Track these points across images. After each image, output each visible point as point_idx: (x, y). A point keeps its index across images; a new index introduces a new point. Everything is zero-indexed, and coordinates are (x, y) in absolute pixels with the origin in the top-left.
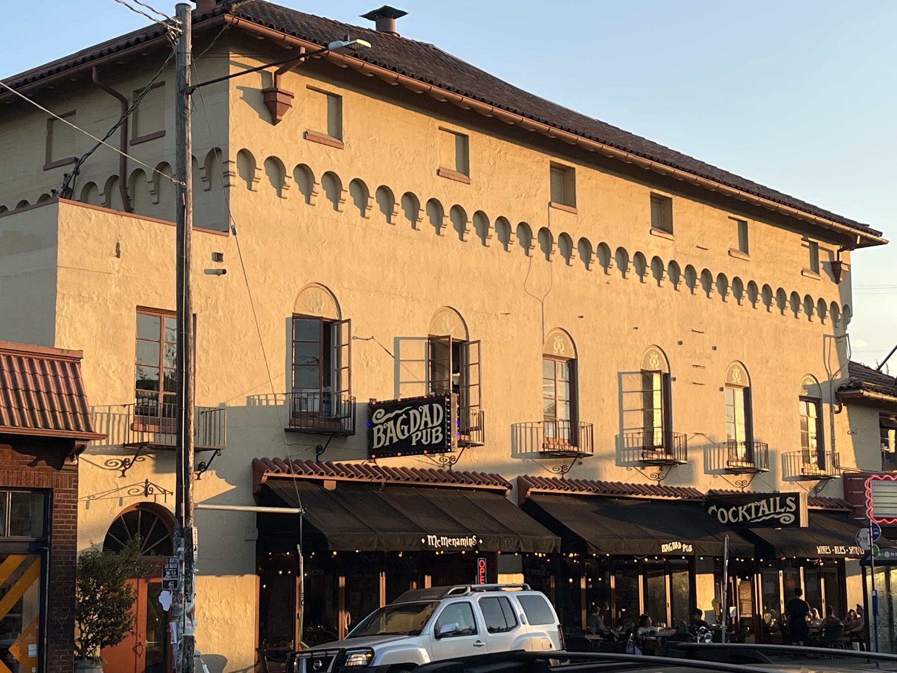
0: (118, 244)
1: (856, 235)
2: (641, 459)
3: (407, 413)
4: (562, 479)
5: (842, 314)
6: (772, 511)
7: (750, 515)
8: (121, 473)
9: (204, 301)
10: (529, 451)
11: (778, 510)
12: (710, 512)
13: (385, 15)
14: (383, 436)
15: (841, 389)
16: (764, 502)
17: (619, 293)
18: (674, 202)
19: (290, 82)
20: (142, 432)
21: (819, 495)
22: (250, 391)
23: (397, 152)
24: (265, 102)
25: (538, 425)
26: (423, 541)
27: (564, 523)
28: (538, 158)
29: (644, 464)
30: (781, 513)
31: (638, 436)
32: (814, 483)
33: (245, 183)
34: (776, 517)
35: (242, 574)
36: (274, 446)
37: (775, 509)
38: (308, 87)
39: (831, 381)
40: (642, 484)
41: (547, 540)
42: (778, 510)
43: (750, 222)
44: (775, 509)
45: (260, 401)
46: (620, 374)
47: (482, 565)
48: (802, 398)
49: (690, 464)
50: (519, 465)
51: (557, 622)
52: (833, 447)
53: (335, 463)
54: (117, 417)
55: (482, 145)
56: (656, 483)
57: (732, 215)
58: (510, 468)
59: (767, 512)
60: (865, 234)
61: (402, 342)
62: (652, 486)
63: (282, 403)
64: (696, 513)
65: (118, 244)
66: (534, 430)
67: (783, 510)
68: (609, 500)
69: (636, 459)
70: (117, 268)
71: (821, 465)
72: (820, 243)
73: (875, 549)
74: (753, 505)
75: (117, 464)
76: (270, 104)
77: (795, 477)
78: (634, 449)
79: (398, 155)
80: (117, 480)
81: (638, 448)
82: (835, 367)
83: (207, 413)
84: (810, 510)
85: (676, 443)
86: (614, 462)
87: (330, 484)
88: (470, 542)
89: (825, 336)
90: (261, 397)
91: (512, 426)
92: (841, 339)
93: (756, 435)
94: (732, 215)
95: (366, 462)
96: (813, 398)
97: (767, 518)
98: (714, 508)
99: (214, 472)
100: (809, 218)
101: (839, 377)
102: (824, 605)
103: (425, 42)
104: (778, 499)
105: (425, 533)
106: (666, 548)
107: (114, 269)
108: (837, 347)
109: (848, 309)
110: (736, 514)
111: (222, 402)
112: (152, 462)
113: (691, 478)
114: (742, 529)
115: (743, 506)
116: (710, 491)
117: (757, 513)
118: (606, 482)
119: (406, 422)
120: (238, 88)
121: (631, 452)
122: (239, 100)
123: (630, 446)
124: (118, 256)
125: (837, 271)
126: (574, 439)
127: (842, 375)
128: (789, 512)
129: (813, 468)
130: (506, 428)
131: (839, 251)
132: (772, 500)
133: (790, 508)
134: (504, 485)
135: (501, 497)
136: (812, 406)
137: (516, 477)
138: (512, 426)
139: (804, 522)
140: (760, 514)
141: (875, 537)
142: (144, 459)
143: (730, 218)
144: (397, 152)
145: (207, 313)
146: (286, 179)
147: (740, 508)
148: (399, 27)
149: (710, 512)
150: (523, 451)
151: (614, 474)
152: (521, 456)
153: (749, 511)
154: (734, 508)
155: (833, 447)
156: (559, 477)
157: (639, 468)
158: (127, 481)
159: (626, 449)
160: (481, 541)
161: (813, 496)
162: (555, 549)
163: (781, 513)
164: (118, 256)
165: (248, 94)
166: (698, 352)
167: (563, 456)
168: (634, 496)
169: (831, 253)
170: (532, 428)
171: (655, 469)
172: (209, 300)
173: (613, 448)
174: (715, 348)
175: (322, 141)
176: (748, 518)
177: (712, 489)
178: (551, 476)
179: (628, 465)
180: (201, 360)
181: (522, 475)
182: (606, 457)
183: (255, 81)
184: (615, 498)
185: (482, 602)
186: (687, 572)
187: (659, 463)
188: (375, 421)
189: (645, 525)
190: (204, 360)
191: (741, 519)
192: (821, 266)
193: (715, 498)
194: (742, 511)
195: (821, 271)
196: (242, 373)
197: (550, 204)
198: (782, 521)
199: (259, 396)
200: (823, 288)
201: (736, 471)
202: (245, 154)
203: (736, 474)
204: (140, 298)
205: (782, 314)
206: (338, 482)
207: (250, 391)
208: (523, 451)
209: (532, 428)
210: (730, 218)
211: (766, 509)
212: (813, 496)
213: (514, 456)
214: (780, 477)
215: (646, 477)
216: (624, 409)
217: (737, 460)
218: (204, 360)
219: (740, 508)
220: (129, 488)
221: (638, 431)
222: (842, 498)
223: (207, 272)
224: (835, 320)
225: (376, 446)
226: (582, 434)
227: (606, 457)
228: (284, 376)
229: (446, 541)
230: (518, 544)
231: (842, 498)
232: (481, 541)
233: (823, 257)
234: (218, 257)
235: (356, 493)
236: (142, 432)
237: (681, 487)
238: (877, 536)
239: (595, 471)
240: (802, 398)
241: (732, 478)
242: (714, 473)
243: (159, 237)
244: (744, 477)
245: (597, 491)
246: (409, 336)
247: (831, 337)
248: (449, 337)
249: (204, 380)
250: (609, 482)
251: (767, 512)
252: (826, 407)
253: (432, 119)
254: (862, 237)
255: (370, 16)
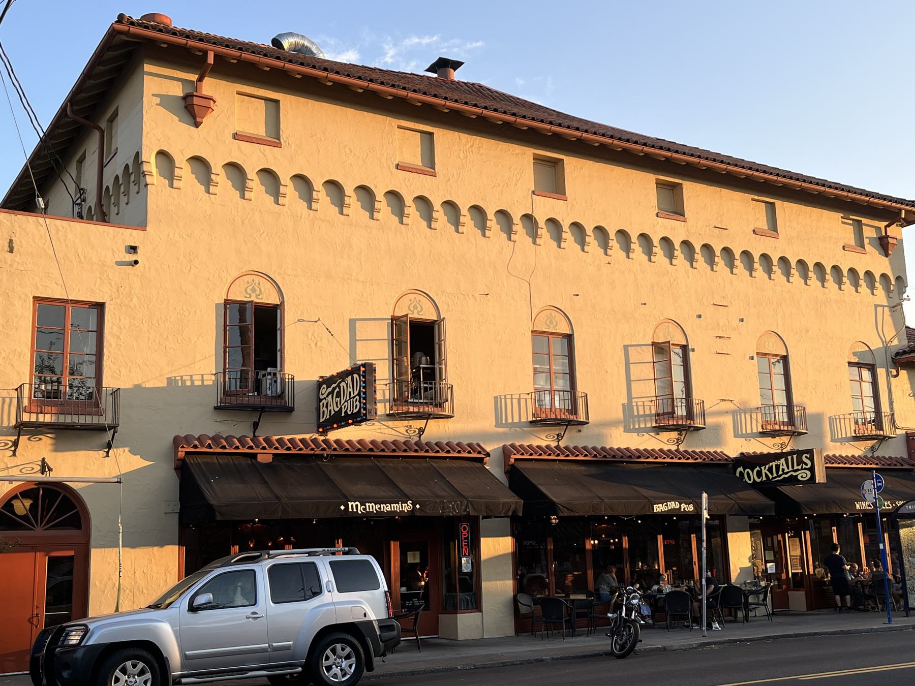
0: (11, 241)
1: (900, 210)
2: (654, 425)
3: (339, 386)
4: (558, 447)
5: (896, 285)
6: (791, 469)
7: (772, 474)
8: (11, 453)
9: (115, 290)
10: (516, 420)
11: (796, 467)
12: (738, 475)
13: (443, 65)
14: (325, 409)
15: (897, 354)
16: (783, 461)
17: (623, 272)
18: (684, 187)
19: (211, 86)
20: (37, 413)
21: (876, 455)
22: (171, 372)
23: (347, 149)
24: (186, 107)
25: (527, 396)
26: (342, 508)
27: (542, 488)
28: (517, 151)
29: (659, 429)
30: (798, 470)
31: (650, 404)
32: (870, 443)
33: (166, 182)
34: (794, 474)
35: (162, 545)
36: (204, 425)
37: (793, 467)
38: (239, 93)
39: (886, 348)
40: (657, 449)
41: (504, 503)
42: (796, 467)
43: (778, 203)
44: (793, 467)
45: (183, 382)
46: (626, 348)
47: (465, 531)
48: (851, 364)
49: (717, 428)
50: (504, 433)
51: (384, 586)
52: (892, 409)
53: (287, 437)
54: (8, 400)
55: (447, 140)
56: (674, 448)
57: (756, 197)
58: (490, 437)
59: (786, 470)
60: (909, 208)
61: (358, 324)
62: (669, 451)
63: (211, 383)
64: (718, 473)
65: (11, 241)
66: (523, 402)
67: (800, 467)
68: (611, 466)
69: (649, 425)
70: (9, 263)
71: (880, 427)
72: (864, 221)
73: (880, 500)
74: (774, 464)
75: (6, 444)
76: (191, 109)
77: (846, 438)
78: (645, 416)
79: (348, 152)
80: (6, 460)
81: (650, 415)
82: (890, 332)
83: (116, 392)
84: (826, 468)
85: (696, 409)
86: (621, 429)
87: (265, 457)
88: (407, 507)
89: (876, 306)
90: (184, 378)
91: (496, 398)
92: (896, 309)
93: (796, 400)
94: (756, 197)
95: (316, 436)
96: (865, 364)
97: (786, 476)
98: (741, 469)
99: (127, 449)
100: (859, 200)
101: (896, 342)
102: (889, 559)
103: (472, 82)
104: (795, 456)
105: (346, 500)
106: (659, 508)
107: (6, 263)
108: (892, 316)
109: (901, 281)
110: (759, 474)
111: (137, 383)
112: (49, 441)
113: (719, 441)
114: (767, 488)
115: (765, 465)
116: (742, 454)
117: (777, 471)
118: (611, 449)
119: (338, 395)
120: (153, 95)
121: (641, 419)
122: (155, 106)
123: (641, 413)
124: (11, 251)
125: (884, 244)
126: (574, 410)
127: (900, 341)
128: (805, 469)
129: (871, 430)
130: (486, 400)
131: (886, 227)
132: (789, 458)
133: (806, 464)
134: (479, 453)
135: (478, 465)
136: (866, 374)
137: (501, 445)
138: (496, 398)
139: (820, 477)
140: (781, 473)
141: (879, 488)
142: (40, 439)
143: (753, 200)
144: (347, 149)
145: (118, 301)
146: (213, 177)
147: (763, 468)
148: (457, 76)
149: (738, 475)
150: (510, 421)
151: (620, 440)
152: (507, 425)
153: (770, 470)
154: (758, 468)
155: (892, 409)
156: (553, 444)
157: (653, 434)
158: (18, 460)
159: (636, 416)
160: (418, 506)
161: (869, 455)
162: (514, 511)
163: (798, 470)
164: (11, 251)
165: (165, 101)
166: (721, 324)
167: (559, 424)
168: (642, 460)
169: (878, 229)
170: (519, 400)
171: (674, 435)
172: (121, 290)
173: (620, 415)
174: (742, 320)
175: (254, 140)
176: (771, 477)
177: (744, 451)
178: (544, 444)
179: (639, 431)
180: (110, 345)
181: (508, 443)
182: (613, 424)
183: (177, 90)
184: (623, 462)
185: (273, 571)
186: (759, 531)
187: (677, 428)
188: (321, 397)
189: (643, 486)
190: (114, 345)
191: (764, 479)
192: (866, 241)
193: (749, 461)
194: (764, 470)
195: (867, 246)
196: (165, 353)
197: (533, 193)
198: (799, 477)
199: (182, 377)
200: (873, 261)
201: (773, 434)
202: (163, 154)
203: (774, 437)
204: (37, 288)
205: (823, 286)
206: (274, 454)
207: (171, 372)
208: (510, 421)
209: (519, 400)
210: (753, 200)
211: (785, 467)
212: (869, 455)
213: (498, 425)
214: (829, 439)
215: (665, 442)
216: (632, 378)
217: (776, 424)
218: (114, 345)
219: (763, 468)
220: (21, 467)
221: (650, 399)
222: (905, 456)
223: (119, 263)
224: (888, 290)
225: (322, 420)
226: (581, 403)
227: (613, 424)
228: (214, 357)
229: (372, 507)
230: (467, 507)
231: (905, 456)
232: (418, 506)
233: (869, 233)
234: (133, 249)
235: (292, 462)
236: (37, 413)
237: (705, 451)
238: (881, 487)
239: (600, 436)
240: (851, 364)
241: (769, 441)
242: (747, 436)
243: (60, 233)
244: (785, 439)
245: (595, 456)
246: (894, 397)
247: (884, 306)
248: (406, 316)
249: (114, 363)
250: (615, 447)
251: (786, 470)
252: (881, 372)
253: (389, 118)
254: (906, 211)
255: (431, 69)
